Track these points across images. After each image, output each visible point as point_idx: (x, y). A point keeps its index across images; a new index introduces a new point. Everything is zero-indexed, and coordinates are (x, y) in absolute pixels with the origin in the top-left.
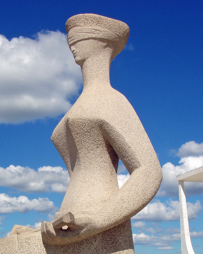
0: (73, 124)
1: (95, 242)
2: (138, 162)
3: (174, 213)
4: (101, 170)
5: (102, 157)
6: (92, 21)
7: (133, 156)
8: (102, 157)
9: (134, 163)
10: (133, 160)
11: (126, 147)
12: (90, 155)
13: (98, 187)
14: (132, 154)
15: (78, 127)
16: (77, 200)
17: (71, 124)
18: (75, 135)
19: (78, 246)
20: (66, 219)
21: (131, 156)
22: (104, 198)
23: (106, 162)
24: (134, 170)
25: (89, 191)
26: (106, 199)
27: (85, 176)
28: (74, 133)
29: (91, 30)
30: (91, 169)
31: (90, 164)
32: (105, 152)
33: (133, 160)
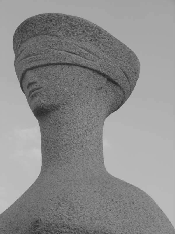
6: (84, 32)
29: (81, 49)
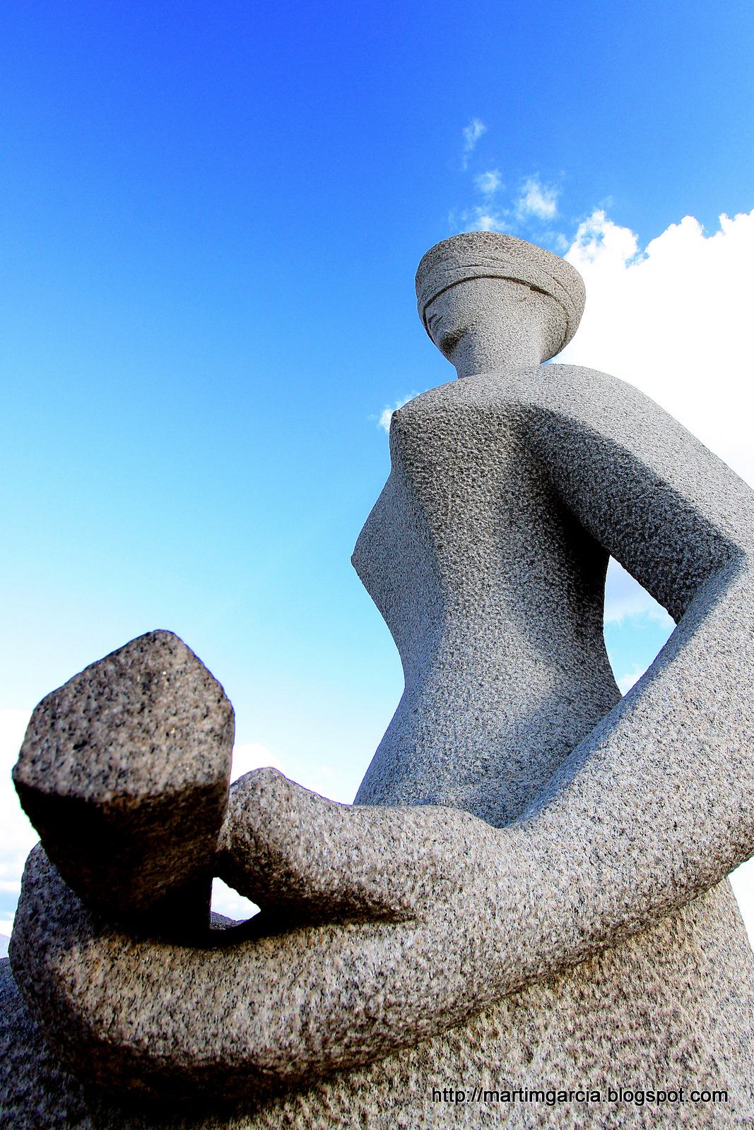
0: (414, 429)
1: (529, 1057)
2: (716, 538)
3: (105, 1038)
4: (530, 613)
5: (533, 562)
7: (683, 515)
8: (533, 562)
9: (692, 551)
10: (686, 536)
11: (644, 485)
12: (481, 552)
13: (524, 686)
14: (678, 507)
15: (433, 442)
16: (419, 749)
17: (405, 433)
18: (418, 472)
19: (382, 1107)
20: (72, 729)
21: (671, 522)
22: (559, 729)
23: (553, 584)
24: (700, 583)
25: (479, 705)
26: (572, 736)
27: (458, 641)
28: (417, 467)
30: (488, 610)
31: (483, 588)
32: (545, 541)
33: (686, 536)
